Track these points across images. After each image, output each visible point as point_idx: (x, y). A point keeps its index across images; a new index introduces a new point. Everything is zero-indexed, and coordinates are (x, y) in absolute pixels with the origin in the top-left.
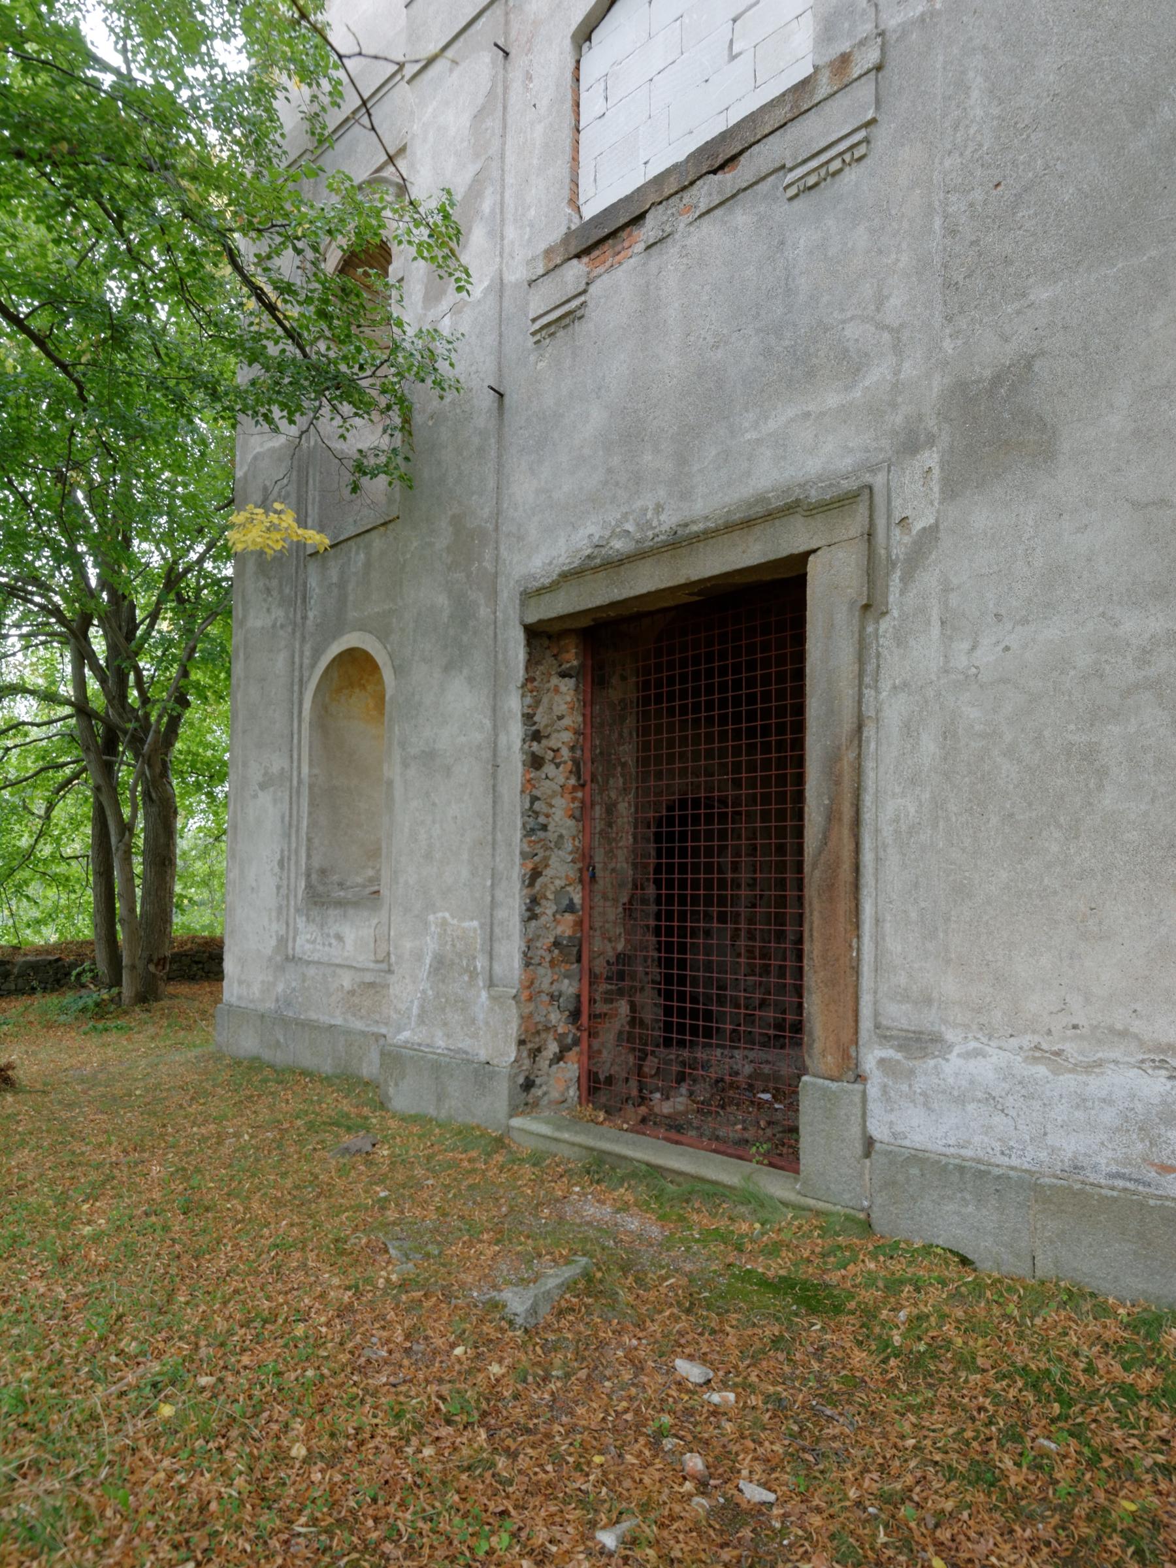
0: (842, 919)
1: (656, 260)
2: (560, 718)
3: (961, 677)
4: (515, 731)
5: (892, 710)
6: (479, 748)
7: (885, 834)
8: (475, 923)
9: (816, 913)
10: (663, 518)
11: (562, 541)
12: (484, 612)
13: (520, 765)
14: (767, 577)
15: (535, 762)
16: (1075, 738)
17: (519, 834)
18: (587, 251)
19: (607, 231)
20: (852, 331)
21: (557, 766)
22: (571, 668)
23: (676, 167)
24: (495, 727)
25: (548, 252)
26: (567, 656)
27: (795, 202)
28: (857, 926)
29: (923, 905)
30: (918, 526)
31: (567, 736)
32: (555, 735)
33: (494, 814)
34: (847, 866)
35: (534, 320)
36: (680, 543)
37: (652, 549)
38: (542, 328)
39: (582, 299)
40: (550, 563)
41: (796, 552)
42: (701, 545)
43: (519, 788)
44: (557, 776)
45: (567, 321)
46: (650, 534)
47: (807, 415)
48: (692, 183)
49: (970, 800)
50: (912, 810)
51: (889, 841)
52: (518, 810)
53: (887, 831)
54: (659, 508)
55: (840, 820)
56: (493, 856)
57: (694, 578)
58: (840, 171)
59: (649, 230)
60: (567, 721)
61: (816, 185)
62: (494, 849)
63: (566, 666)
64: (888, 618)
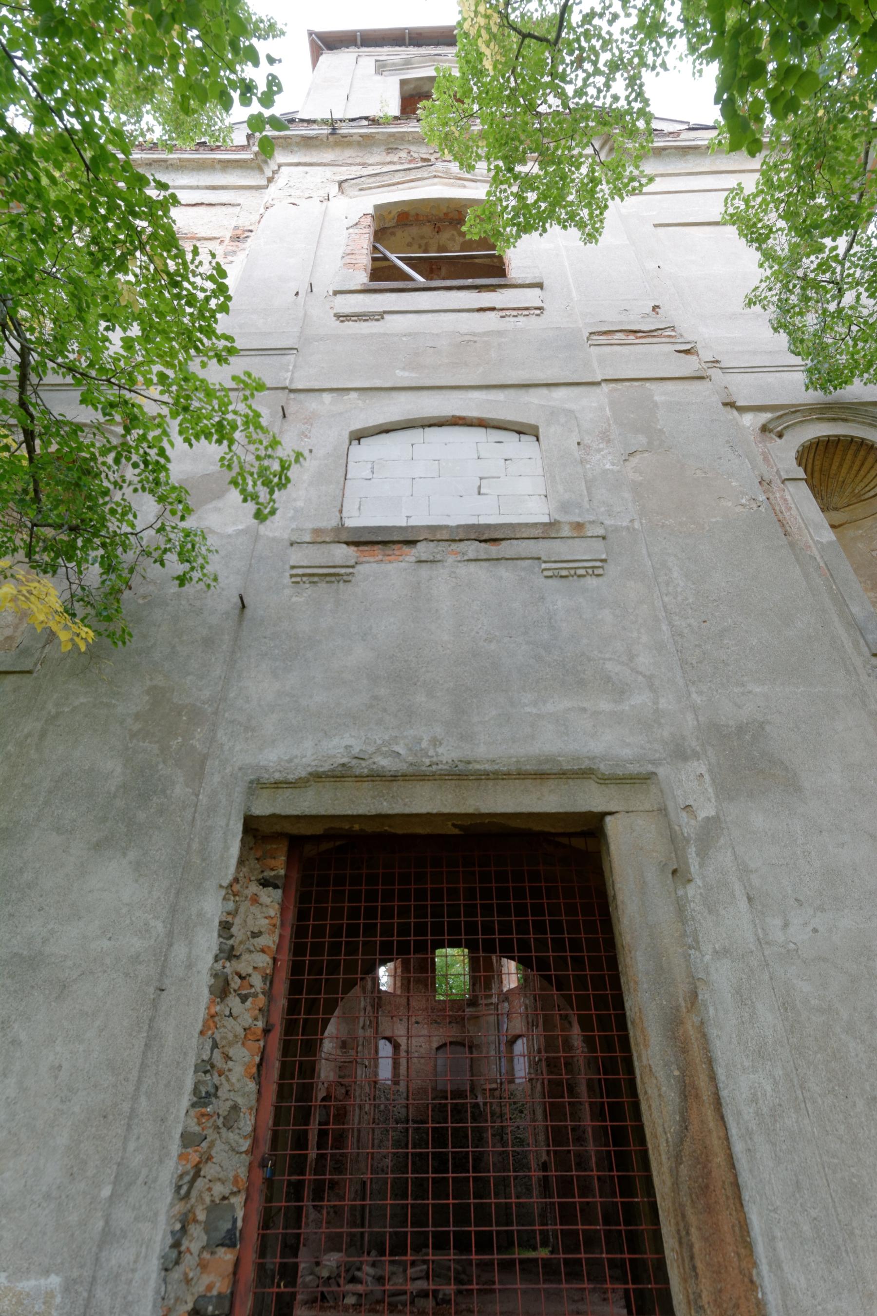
0: (729, 1239)
1: (424, 571)
2: (255, 935)
3: (783, 951)
4: (207, 943)
5: (722, 977)
6: (136, 959)
7: (746, 1117)
8: (54, 1281)
9: (693, 1230)
10: (440, 750)
11: (308, 744)
12: (180, 790)
13: (206, 991)
14: (537, 827)
15: (222, 989)
16: (689, 1026)
17: (185, 1101)
18: (357, 544)
19: (380, 539)
20: (609, 666)
21: (244, 999)
22: (276, 877)
23: (447, 527)
24: (170, 934)
25: (317, 531)
26: (272, 863)
27: (550, 581)
28: (749, 1246)
29: (813, 1213)
30: (702, 815)
31: (263, 961)
32: (246, 957)
33: (143, 1066)
34: (720, 1159)
35: (293, 567)
36: (460, 776)
37: (434, 774)
38: (304, 575)
39: (351, 570)
40: (290, 761)
41: (595, 810)
42: (491, 783)
43: (199, 1026)
44: (245, 1015)
45: (333, 579)
46: (427, 761)
47: (584, 710)
48: (461, 540)
49: (829, 1080)
50: (769, 1088)
51: (753, 1125)
52: (192, 1060)
53: (748, 1113)
54: (435, 742)
55: (697, 1096)
56: (126, 1139)
57: (484, 810)
58: (584, 576)
59: (422, 550)
60: (262, 941)
61: (566, 577)
62: (129, 1127)
63: (268, 874)
64: (692, 885)
